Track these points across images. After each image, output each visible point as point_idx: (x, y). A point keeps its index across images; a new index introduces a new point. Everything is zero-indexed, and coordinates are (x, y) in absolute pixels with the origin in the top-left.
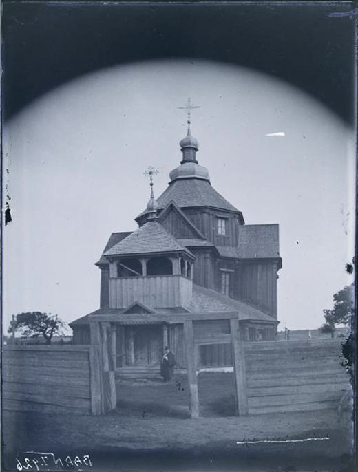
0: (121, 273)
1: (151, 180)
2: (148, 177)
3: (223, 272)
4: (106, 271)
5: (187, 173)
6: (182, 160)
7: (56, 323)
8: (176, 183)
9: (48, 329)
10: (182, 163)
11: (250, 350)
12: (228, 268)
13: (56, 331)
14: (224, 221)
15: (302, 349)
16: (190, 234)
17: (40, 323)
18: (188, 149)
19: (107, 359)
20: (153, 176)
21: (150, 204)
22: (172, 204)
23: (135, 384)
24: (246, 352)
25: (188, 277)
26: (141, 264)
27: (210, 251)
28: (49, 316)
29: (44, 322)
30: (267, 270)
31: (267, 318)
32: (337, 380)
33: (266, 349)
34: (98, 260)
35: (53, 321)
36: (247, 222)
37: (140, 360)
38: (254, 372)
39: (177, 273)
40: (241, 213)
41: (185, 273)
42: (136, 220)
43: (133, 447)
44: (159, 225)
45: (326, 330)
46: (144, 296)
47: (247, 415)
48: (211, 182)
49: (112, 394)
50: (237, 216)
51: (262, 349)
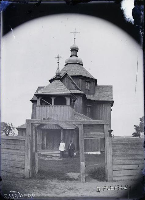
0: (42, 103)
1: (58, 60)
2: (57, 59)
3: (88, 106)
4: (35, 104)
5: (73, 60)
6: (71, 55)
7: (11, 127)
8: (68, 65)
9: (7, 130)
10: (71, 56)
11: (115, 142)
13: (11, 131)
14: (88, 83)
15: (123, 144)
16: (74, 88)
17: (4, 127)
18: (75, 50)
21: (58, 72)
22: (66, 73)
23: (46, 159)
26: (52, 100)
27: (82, 96)
29: (6, 127)
30: (107, 106)
33: (123, 142)
34: (31, 99)
35: (10, 126)
36: (98, 84)
37: (49, 147)
39: (69, 105)
40: (96, 80)
42: (49, 81)
44: (61, 82)
45: (136, 135)
46: (52, 115)
49: (36, 165)
50: (94, 81)
51: (122, 143)
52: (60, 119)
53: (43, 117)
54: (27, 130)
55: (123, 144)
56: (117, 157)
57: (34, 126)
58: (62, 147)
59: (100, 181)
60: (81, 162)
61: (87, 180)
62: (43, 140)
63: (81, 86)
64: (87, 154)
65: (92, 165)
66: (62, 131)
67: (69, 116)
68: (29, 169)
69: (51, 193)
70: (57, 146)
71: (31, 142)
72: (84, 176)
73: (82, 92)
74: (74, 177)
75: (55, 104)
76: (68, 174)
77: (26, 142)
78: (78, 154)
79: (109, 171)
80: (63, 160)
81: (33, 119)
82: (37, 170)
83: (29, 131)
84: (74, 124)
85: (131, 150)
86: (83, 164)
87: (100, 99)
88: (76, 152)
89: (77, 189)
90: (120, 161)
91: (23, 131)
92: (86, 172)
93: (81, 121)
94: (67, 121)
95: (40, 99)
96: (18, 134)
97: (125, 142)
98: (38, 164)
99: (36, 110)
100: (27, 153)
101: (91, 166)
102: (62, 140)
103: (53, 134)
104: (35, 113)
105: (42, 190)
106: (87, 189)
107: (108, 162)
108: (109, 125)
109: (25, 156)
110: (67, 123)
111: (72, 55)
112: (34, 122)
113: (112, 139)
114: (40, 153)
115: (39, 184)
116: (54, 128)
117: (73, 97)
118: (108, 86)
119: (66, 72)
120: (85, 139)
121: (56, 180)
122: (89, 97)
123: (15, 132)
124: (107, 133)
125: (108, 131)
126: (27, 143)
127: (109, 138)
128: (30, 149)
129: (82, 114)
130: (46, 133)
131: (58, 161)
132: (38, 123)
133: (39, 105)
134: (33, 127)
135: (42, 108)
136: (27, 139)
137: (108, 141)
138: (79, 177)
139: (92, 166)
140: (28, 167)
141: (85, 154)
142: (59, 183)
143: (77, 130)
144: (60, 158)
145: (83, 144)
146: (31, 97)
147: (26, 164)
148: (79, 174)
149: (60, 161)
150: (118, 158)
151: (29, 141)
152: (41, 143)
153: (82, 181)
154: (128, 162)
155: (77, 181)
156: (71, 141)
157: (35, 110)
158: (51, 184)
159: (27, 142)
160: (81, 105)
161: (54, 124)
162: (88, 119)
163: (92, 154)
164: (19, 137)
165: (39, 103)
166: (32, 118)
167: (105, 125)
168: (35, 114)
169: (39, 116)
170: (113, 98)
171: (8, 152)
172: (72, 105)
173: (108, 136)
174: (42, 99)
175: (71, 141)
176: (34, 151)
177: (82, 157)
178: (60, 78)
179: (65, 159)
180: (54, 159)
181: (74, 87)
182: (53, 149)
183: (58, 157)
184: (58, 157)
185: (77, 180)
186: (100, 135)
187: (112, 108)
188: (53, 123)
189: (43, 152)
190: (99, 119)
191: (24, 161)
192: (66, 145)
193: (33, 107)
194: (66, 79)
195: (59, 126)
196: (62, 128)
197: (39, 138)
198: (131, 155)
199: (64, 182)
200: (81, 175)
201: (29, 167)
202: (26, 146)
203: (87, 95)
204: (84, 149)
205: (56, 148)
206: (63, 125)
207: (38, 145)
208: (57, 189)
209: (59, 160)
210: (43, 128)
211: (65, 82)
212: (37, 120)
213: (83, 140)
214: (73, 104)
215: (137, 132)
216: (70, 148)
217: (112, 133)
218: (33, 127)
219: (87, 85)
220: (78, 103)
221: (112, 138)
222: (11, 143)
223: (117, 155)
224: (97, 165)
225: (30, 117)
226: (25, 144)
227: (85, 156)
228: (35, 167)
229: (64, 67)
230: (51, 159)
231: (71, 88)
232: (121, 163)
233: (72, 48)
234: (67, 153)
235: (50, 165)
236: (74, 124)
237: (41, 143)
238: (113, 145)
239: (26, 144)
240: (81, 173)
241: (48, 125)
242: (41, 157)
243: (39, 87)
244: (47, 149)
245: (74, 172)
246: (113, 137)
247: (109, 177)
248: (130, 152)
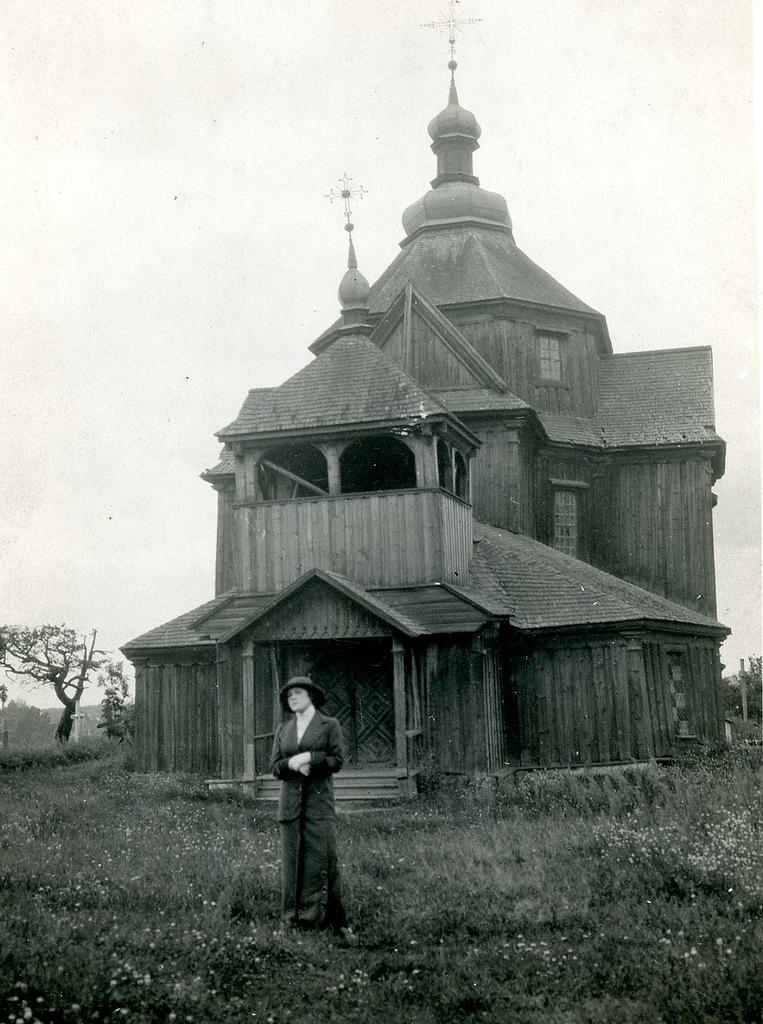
1: (348, 215)
12: (570, 477)
14: (555, 343)
18: (455, 140)
20: (354, 202)
25: (459, 495)
31: (687, 614)
32: (658, 745)
36: (619, 346)
41: (453, 483)
59: (509, 218)
66: (396, 648)
116: (348, 636)
174: (269, 463)
196: (399, 635)
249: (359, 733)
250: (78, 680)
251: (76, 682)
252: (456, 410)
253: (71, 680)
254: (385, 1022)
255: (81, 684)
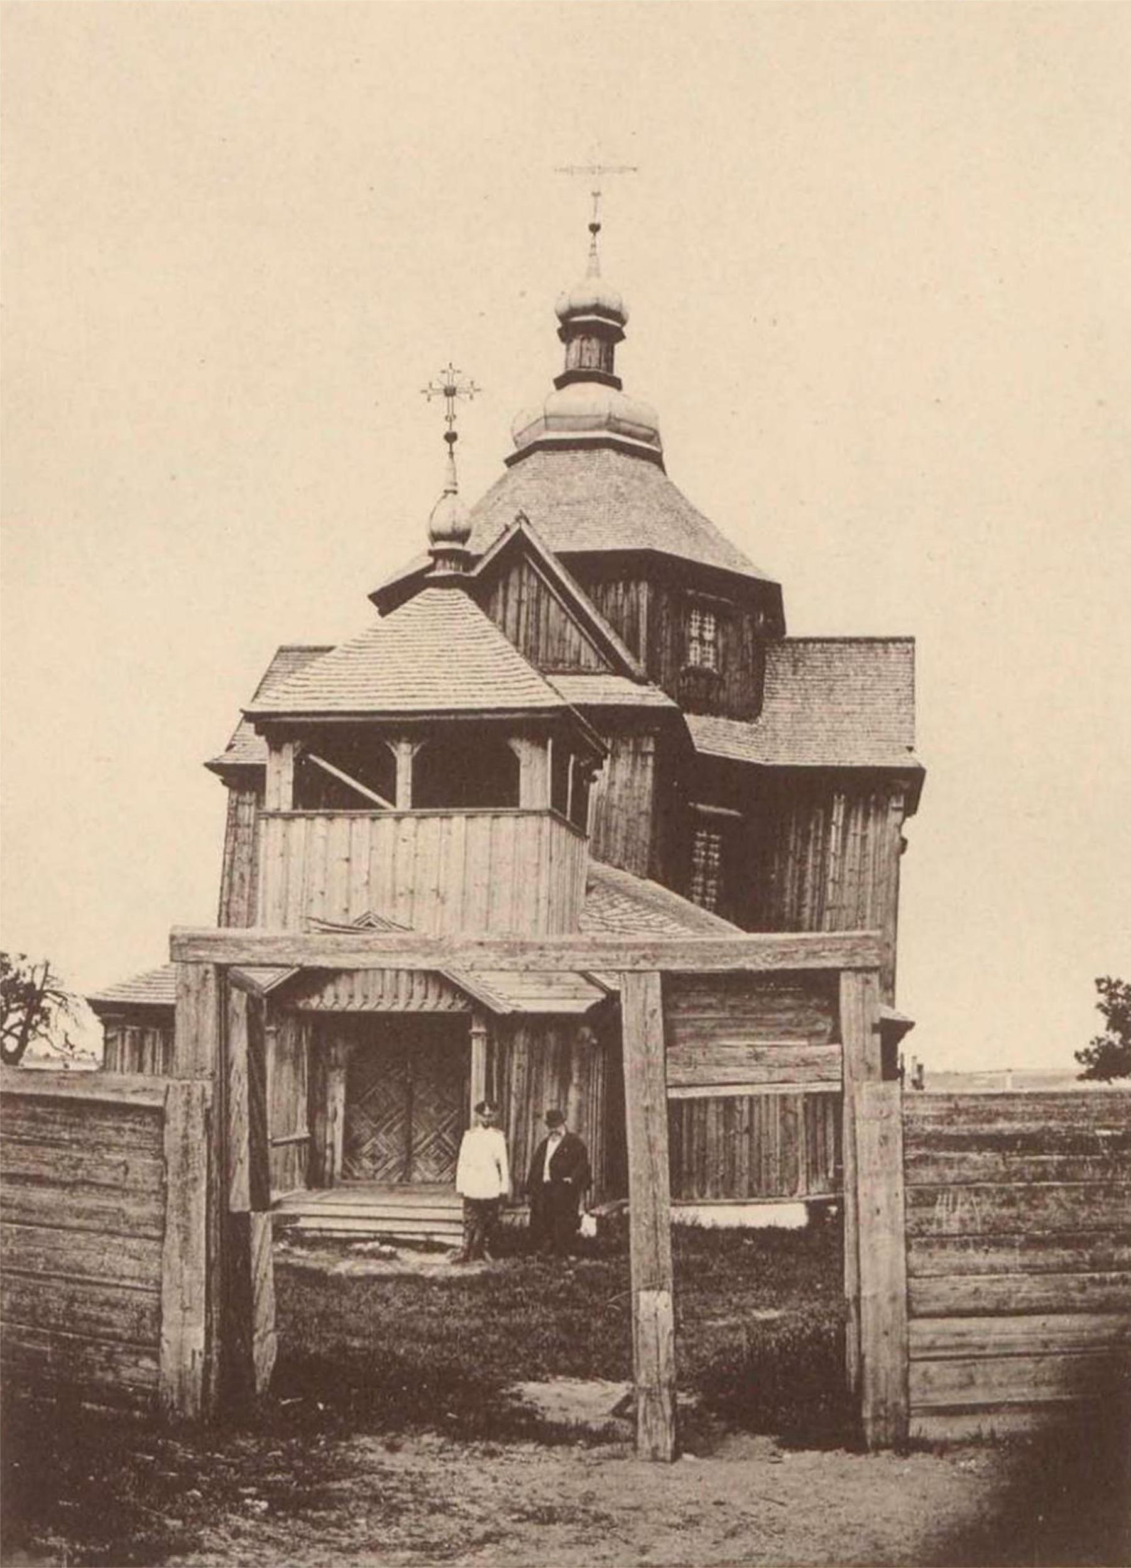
1: (450, 418)
4: (249, 797)
6: (560, 371)
7: (42, 994)
8: (536, 460)
10: (561, 382)
13: (41, 1028)
16: (588, 656)
18: (593, 332)
19: (244, 1150)
20: (460, 404)
21: (444, 524)
23: (343, 1267)
24: (910, 1139)
28: (17, 965)
34: (217, 752)
35: (32, 985)
36: (795, 628)
37: (366, 1163)
38: (943, 1240)
42: (375, 597)
43: (256, 1242)
44: (467, 604)
46: (394, 897)
47: (906, 1446)
48: (665, 458)
49: (259, 1318)
51: (987, 1129)
52: (463, 928)
53: (316, 914)
54: (179, 1020)
55: (999, 1143)
56: (943, 1246)
57: (243, 985)
58: (483, 1164)
60: (644, 1296)
61: (695, 1436)
62: (317, 1109)
63: (643, 642)
64: (697, 1229)
65: (733, 1320)
67: (543, 903)
68: (200, 1346)
69: (383, 1546)
70: (438, 1159)
71: (217, 1122)
72: (668, 1411)
73: (656, 697)
74: (583, 1417)
75: (415, 804)
76: (531, 1388)
77: (176, 1123)
78: (615, 1232)
79: (875, 1371)
80: (485, 1276)
81: (232, 932)
82: (265, 1349)
83: (197, 1024)
84: (581, 966)
85: (1062, 1194)
86: (655, 1307)
87: (811, 757)
88: (602, 1210)
89: (606, 1517)
90: (971, 1282)
91: (143, 1034)
92: (680, 1376)
93: (636, 947)
94: (524, 947)
95: (288, 753)
96: (100, 1056)
97: (1017, 1126)
98: (279, 1310)
99: (254, 845)
100: (185, 1212)
101: (721, 1323)
102: (480, 1109)
103: (403, 1061)
104: (254, 876)
105: (305, 1519)
106: (692, 1510)
107: (866, 1292)
108: (886, 978)
109: (161, 1239)
110: (522, 960)
111: (571, 367)
112: (244, 957)
113: (904, 1097)
114: (295, 1218)
115: (279, 1470)
116: (413, 1008)
117: (579, 738)
118: (832, 641)
119: (521, 517)
120: (674, 1094)
121: (426, 1439)
122: (713, 736)
123: (72, 1040)
124: (860, 1042)
125: (875, 1028)
126: (185, 1136)
127: (882, 1086)
128: (204, 1188)
129: (651, 875)
130: (340, 1051)
131: (448, 1284)
132: (278, 959)
133: (286, 808)
134: (235, 993)
135: (309, 837)
136: (175, 1091)
137: (872, 1119)
138: (618, 1411)
139: (734, 1329)
140: (187, 1337)
141: (677, 1229)
142: (451, 1466)
143: (607, 1015)
144: (464, 1261)
145: (663, 1143)
146: (220, 731)
147: (171, 1313)
148: (620, 1390)
149: (462, 1279)
150: (956, 1261)
151: (199, 1119)
152: (303, 1132)
153: (645, 1444)
154: (1031, 1288)
155: (606, 1449)
156: (555, 1119)
157: (245, 852)
158: (387, 1476)
159: (185, 1129)
160: (646, 805)
161: (411, 973)
162: (700, 927)
163: (735, 1223)
164: (114, 1077)
165: (288, 792)
166: (226, 916)
167: (843, 975)
168: (253, 887)
169: (283, 905)
170: (917, 745)
171: (20, 1207)
172: (569, 808)
173: (870, 1069)
175: (555, 1119)
176: (240, 1198)
177: (649, 1249)
178: (488, 573)
179: (502, 1265)
180: (407, 1270)
181: (584, 644)
182: (403, 1179)
183: (442, 1248)
184: (442, 1248)
185: (605, 1436)
186: (806, 1063)
187: (912, 828)
188: (405, 962)
189: (318, 1210)
190: (797, 927)
191: (159, 1284)
192: (515, 1151)
193: (234, 823)
194: (519, 590)
195: (458, 991)
196: (478, 1008)
197: (284, 1091)
198: (1063, 1238)
199: (491, 1454)
200: (642, 1399)
201: (197, 1337)
202: (174, 1160)
203: (694, 722)
204: (664, 1181)
205: (430, 1177)
206: (487, 977)
207: (274, 1153)
208: (434, 1509)
209: (456, 1271)
210: (314, 1002)
211: (512, 603)
212: (266, 935)
213: (661, 1107)
214: (581, 795)
215: (1116, 1038)
216: (547, 1177)
217: (907, 1047)
218: (235, 993)
219: (695, 633)
220: (616, 791)
221: (908, 1088)
222: (47, 1131)
223: (945, 1229)
224: (773, 1314)
225: (201, 914)
226: (159, 1139)
227: (675, 1245)
228: (254, 1330)
229: (502, 482)
230: (386, 1269)
231: (556, 662)
232: (984, 1303)
233: (573, 311)
234: (522, 1216)
235: (375, 1318)
236: (583, 974)
237: (303, 1132)
238: (922, 1145)
239: (172, 1141)
240: (642, 1379)
241: (359, 978)
242: (304, 1253)
243: (282, 650)
244: (348, 1179)
245: (584, 1373)
246: (918, 1084)
247: (876, 1418)
248: (1054, 1210)
249: (414, 1142)
250: (20, 1028)
251: (17, 1031)
252: (576, 701)
253: (12, 1027)
254: (991, 1565)
255: (24, 1033)
